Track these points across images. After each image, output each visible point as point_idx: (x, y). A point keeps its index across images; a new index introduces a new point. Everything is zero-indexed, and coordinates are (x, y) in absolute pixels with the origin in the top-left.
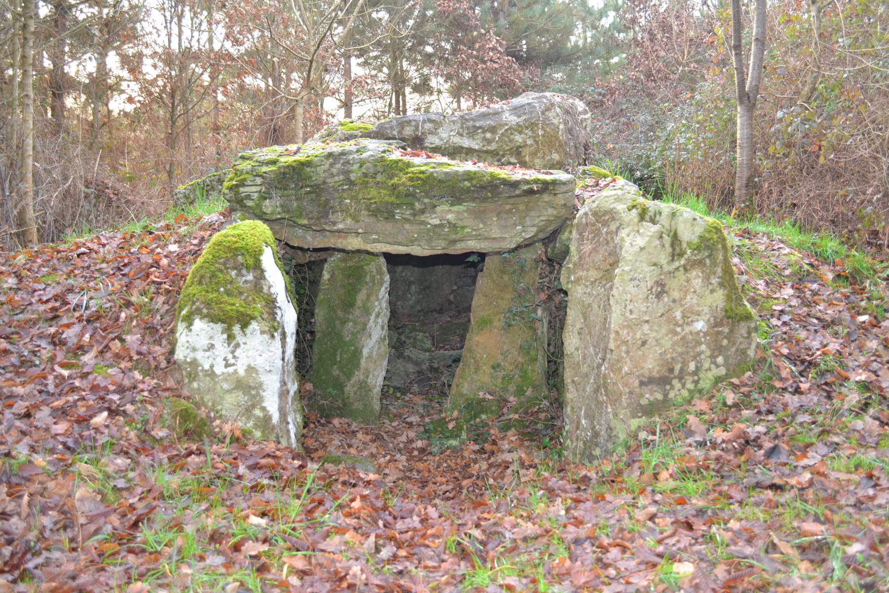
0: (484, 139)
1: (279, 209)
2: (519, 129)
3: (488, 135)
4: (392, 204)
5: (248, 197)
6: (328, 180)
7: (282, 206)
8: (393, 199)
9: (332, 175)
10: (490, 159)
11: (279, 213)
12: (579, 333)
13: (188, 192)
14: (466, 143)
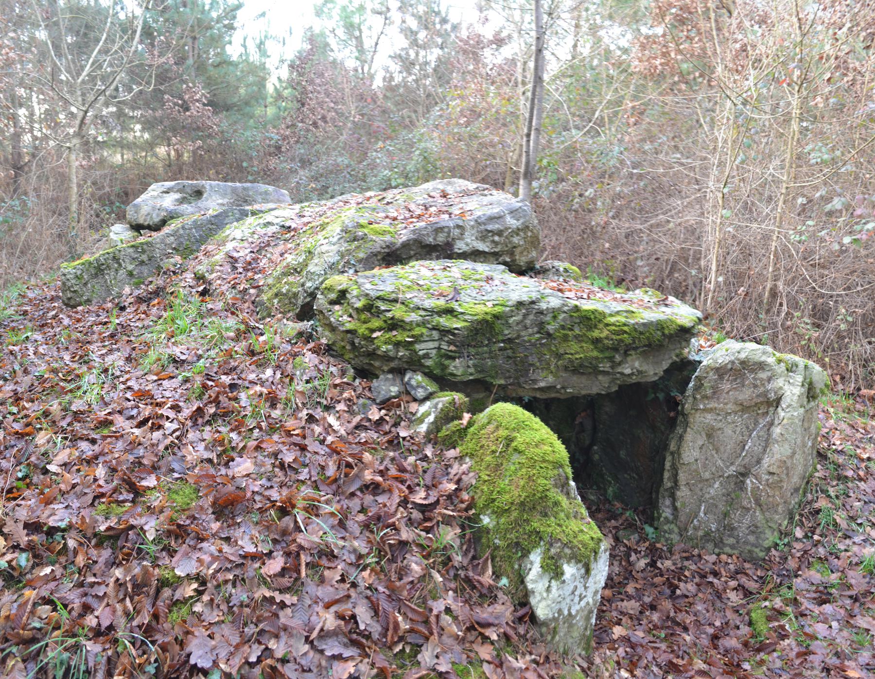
0: (493, 241)
1: (472, 370)
2: (517, 232)
3: (496, 238)
4: (597, 358)
5: (426, 356)
6: (523, 334)
7: (475, 366)
8: (595, 353)
9: (526, 328)
10: (492, 259)
11: (471, 374)
12: (701, 448)
13: (79, 272)
14: (482, 246)
